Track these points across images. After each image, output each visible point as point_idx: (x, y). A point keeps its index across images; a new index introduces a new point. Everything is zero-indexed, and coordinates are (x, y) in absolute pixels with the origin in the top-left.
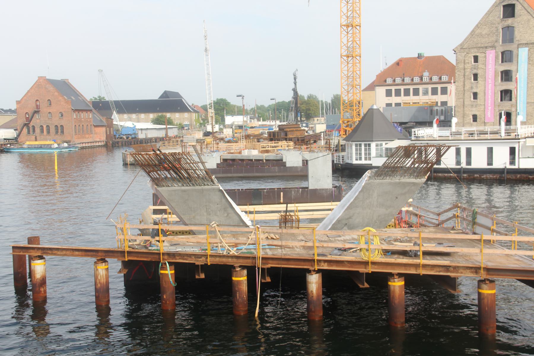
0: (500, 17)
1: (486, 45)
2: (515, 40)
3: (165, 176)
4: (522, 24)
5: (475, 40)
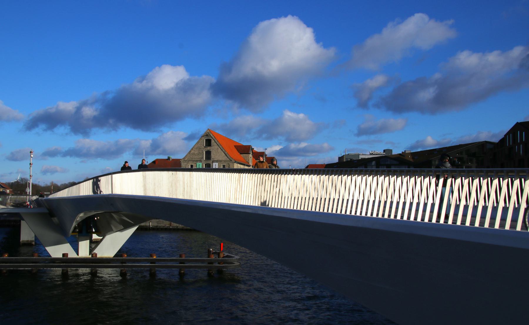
1: (197, 160)
2: (211, 158)
5: (191, 156)
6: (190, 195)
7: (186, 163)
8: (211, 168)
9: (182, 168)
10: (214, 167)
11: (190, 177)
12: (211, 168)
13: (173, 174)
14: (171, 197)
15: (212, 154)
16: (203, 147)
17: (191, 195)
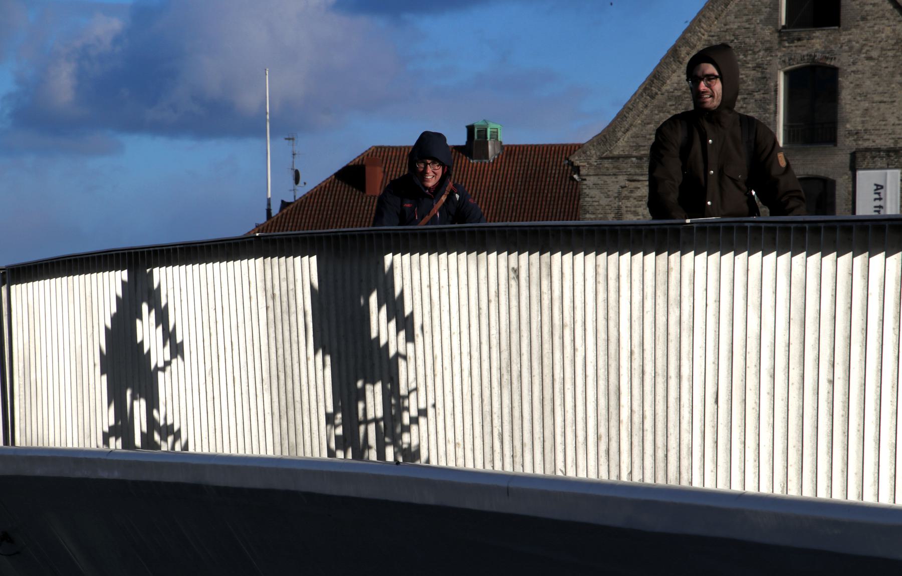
0: (777, 19)
2: (841, 132)
3: (337, 181)
4: (870, 58)
6: (660, 454)
7: (622, 180)
8: (841, 212)
9: (589, 219)
10: (865, 208)
11: (661, 301)
12: (841, 212)
13: (517, 271)
14: (503, 465)
15: (846, 96)
16: (767, 33)
17: (673, 443)
